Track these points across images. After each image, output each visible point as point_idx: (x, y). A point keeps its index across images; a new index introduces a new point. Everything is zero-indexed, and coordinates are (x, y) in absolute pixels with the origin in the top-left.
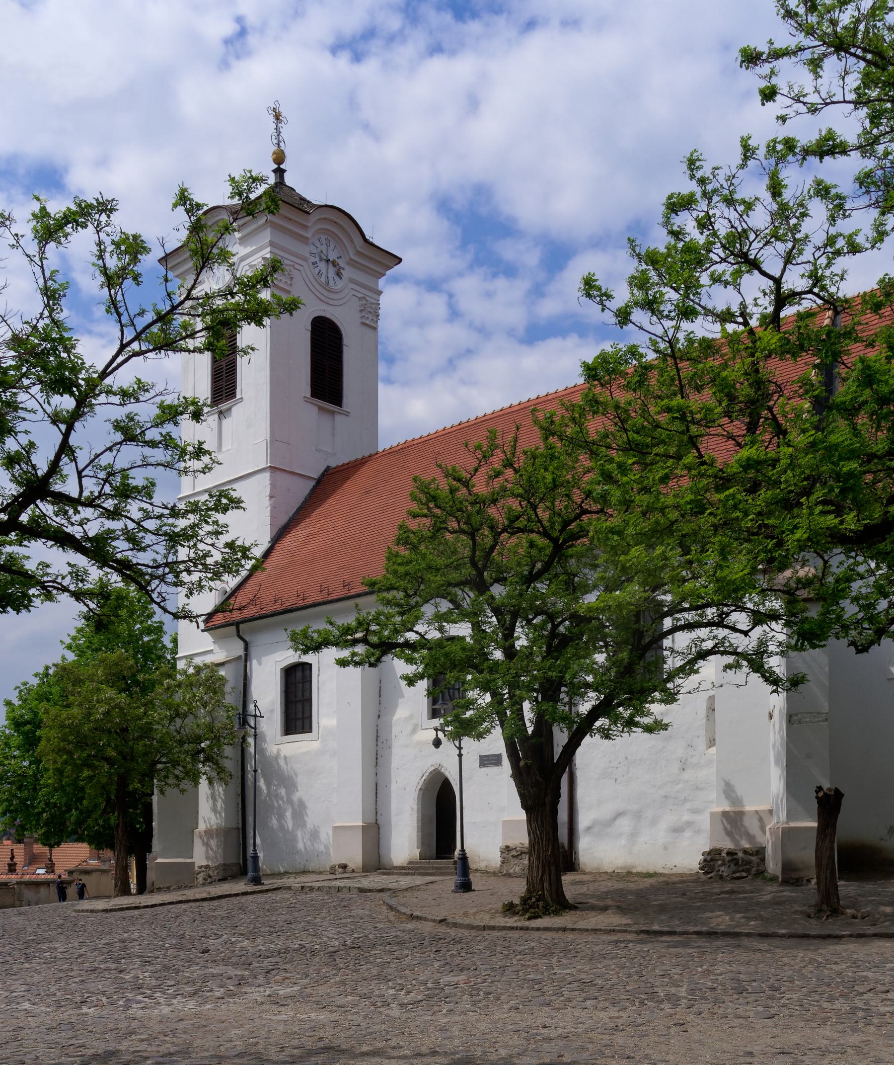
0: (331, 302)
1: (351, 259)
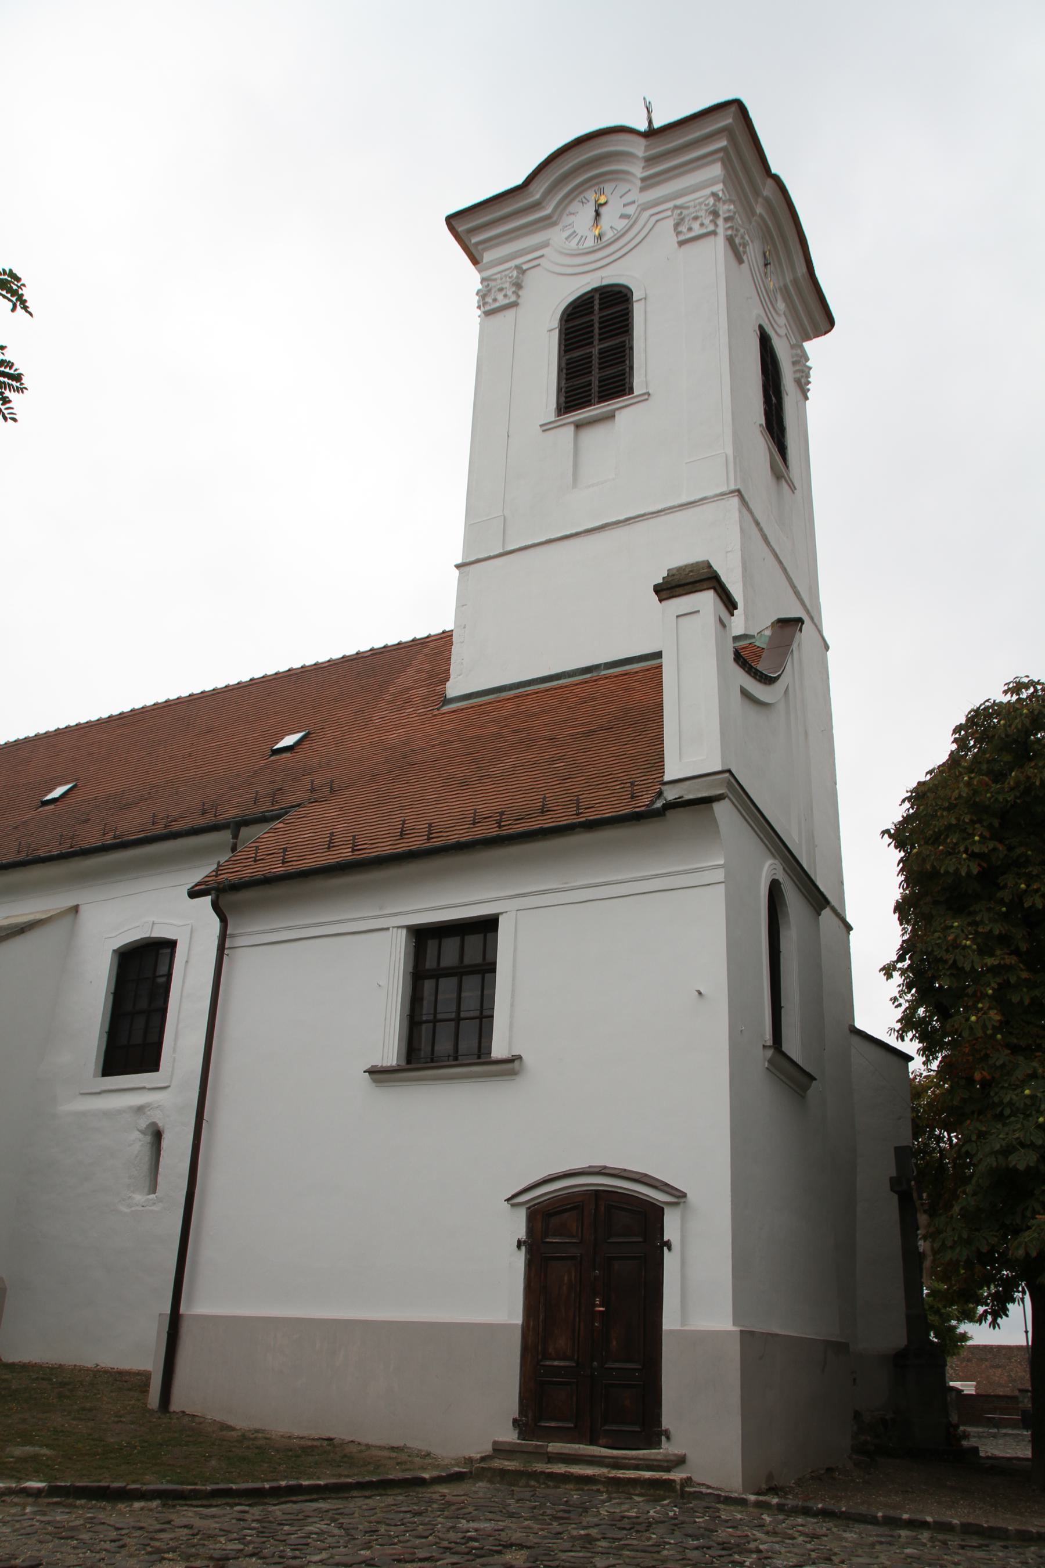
0: (775, 326)
1: (786, 286)
